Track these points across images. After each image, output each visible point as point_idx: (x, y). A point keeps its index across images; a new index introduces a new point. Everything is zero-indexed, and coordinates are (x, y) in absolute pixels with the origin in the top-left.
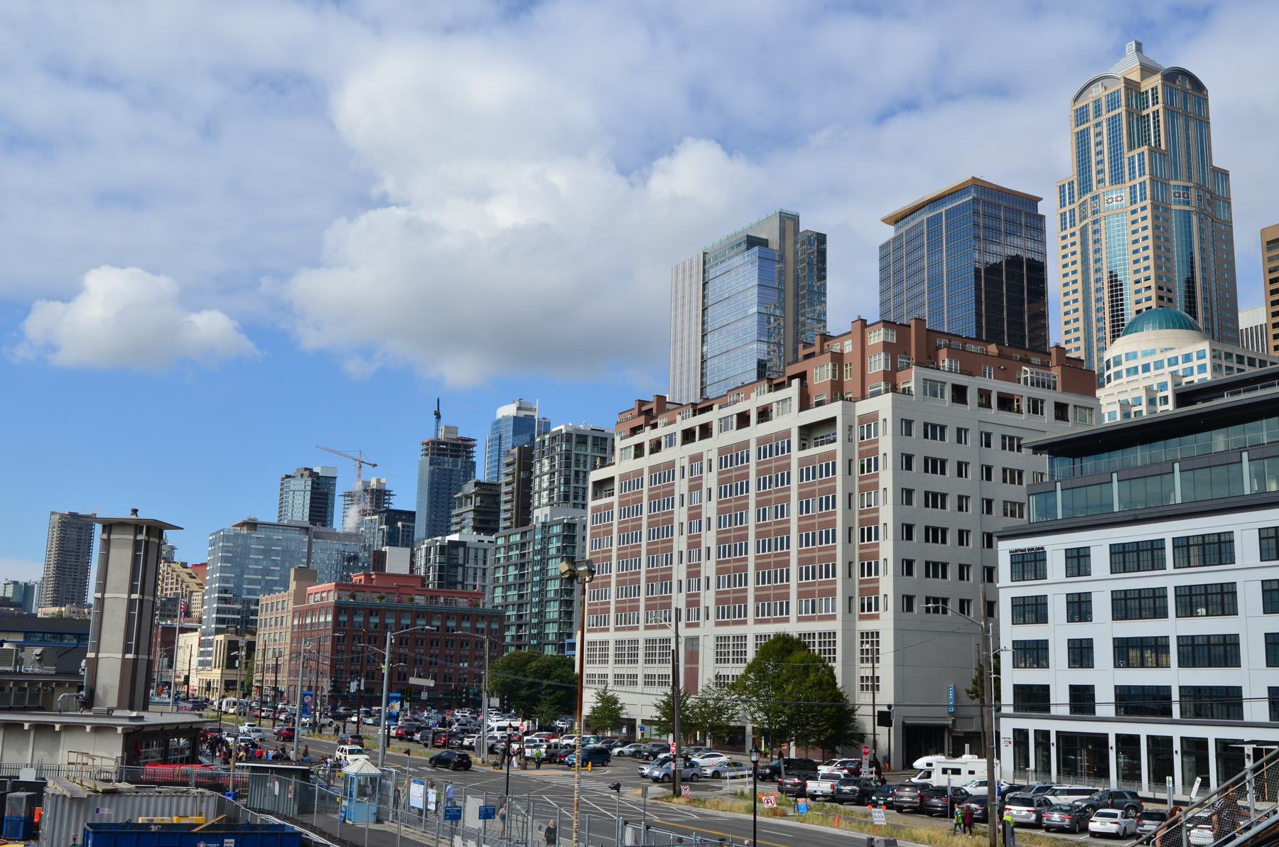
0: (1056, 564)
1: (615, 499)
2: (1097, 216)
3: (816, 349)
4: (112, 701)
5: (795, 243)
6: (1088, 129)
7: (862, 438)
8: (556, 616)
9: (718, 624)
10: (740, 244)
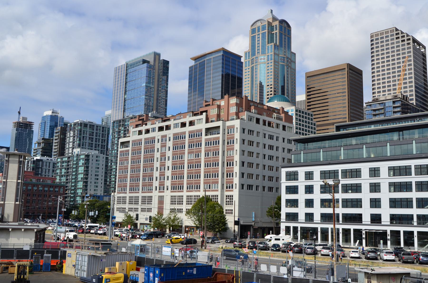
0: (302, 176)
1: (130, 148)
2: (257, 64)
3: (211, 103)
4: (11, 219)
5: (159, 63)
6: (255, 35)
7: (228, 133)
8: (81, 186)
9: (171, 192)
10: (139, 62)
